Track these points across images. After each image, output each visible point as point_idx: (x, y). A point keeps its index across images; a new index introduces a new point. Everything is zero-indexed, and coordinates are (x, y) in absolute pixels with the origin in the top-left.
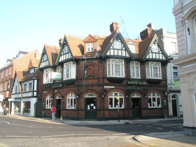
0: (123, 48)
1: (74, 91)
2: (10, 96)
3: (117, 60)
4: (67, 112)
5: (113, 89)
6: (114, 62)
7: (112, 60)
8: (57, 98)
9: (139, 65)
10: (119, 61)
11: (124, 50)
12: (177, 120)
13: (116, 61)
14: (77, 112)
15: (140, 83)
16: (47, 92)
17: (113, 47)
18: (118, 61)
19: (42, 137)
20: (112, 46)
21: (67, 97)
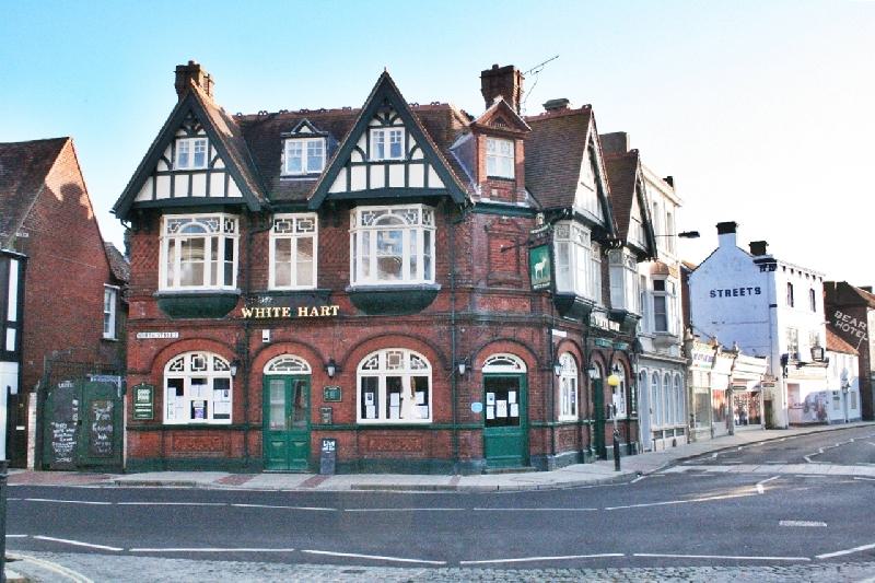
0: (414, 149)
4: (363, 439)
9: (433, 222)
12: (746, 484)
13: (190, 220)
14: (237, 438)
15: (303, 312)
16: (175, 335)
17: (170, 166)
18: (198, 220)
19: (825, 560)
20: (167, 161)
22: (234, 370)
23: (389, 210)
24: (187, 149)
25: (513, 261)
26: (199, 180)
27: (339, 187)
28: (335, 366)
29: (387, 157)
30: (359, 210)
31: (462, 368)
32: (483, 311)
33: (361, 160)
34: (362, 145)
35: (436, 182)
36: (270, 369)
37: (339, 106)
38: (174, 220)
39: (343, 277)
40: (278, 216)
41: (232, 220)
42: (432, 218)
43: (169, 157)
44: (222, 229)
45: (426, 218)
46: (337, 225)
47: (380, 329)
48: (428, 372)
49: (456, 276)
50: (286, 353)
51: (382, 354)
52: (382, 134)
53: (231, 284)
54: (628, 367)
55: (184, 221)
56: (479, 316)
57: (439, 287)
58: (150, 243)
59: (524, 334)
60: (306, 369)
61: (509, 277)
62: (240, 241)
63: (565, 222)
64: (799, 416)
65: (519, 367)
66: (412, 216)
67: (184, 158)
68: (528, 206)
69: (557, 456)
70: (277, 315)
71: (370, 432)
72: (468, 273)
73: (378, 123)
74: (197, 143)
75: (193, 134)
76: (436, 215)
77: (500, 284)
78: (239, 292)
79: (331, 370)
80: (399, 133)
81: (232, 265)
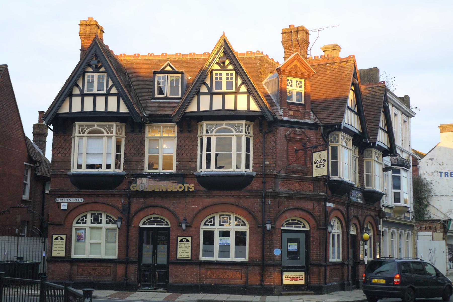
2: (438, 226)
3: (224, 122)
5: (81, 204)
6: (215, 130)
7: (80, 126)
8: (141, 225)
9: (124, 134)
11: (243, 93)
13: (94, 126)
16: (81, 200)
18: (98, 126)
20: (207, 86)
21: (75, 225)
22: (119, 224)
23: (96, 125)
24: (221, 78)
25: (303, 158)
26: (101, 101)
27: (193, 108)
29: (95, 91)
32: (282, 189)
33: (207, 91)
35: (124, 109)
36: (143, 224)
38: (82, 126)
39: (193, 165)
41: (249, 126)
43: (81, 86)
44: (244, 132)
45: (248, 130)
46: (189, 132)
47: (215, 200)
48: (246, 228)
49: (265, 166)
50: (154, 213)
52: (93, 76)
53: (119, 168)
54: (375, 226)
56: (280, 193)
57: (255, 174)
58: (65, 140)
59: (309, 205)
61: (299, 168)
63: (337, 133)
67: (91, 85)
69: (328, 285)
73: (91, 70)
74: (227, 74)
75: (97, 70)
78: (125, 173)
79: (184, 226)
80: (103, 76)
81: (249, 155)
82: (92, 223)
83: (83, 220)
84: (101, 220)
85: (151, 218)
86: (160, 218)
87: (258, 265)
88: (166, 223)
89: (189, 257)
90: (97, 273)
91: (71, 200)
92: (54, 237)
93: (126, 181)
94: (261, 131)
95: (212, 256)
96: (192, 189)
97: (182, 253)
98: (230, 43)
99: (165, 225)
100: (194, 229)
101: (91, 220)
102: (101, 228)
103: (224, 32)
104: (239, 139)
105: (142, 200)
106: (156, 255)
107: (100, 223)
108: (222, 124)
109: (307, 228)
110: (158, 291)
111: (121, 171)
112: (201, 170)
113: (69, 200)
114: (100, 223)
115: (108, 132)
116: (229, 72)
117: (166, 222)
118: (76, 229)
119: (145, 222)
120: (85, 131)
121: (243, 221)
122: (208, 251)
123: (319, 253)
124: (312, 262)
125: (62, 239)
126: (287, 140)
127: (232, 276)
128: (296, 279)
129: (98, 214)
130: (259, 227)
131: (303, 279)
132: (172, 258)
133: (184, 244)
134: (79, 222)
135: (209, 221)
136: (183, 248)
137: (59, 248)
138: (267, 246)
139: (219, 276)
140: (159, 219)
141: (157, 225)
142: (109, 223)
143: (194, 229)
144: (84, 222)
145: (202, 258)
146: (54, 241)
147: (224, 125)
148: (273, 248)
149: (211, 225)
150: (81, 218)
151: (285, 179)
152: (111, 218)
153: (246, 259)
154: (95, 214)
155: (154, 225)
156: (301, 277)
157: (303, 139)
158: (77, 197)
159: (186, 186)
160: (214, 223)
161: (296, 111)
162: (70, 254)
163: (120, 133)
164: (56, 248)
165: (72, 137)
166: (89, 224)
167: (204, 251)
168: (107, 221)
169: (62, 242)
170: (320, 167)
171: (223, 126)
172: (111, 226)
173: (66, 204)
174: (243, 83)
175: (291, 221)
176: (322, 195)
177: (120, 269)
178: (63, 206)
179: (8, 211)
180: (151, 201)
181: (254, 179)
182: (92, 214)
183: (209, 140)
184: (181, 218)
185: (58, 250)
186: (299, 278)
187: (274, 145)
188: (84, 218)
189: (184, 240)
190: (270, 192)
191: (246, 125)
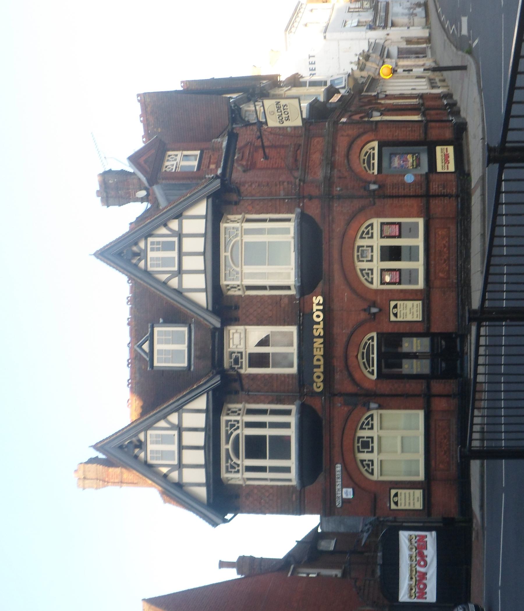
0: (169, 422)
1: (348, 223)
3: (223, 254)
4: (437, 283)
5: (345, 468)
8: (375, 377)
10: (228, 436)
11: (180, 419)
13: (227, 450)
16: (338, 468)
18: (227, 442)
20: (169, 279)
28: (370, 307)
30: (224, 475)
31: (373, 187)
32: (320, 174)
34: (164, 470)
36: (372, 373)
37: (128, 328)
38: (227, 468)
39: (286, 301)
40: (226, 365)
41: (229, 409)
42: (230, 217)
44: (238, 418)
45: (235, 412)
47: (336, 267)
50: (357, 357)
51: (360, 265)
55: (228, 457)
57: (299, 210)
59: (342, 143)
60: (372, 338)
62: (249, 403)
64: (420, 18)
65: (372, 338)
66: (232, 426)
67: (166, 262)
68: (227, 138)
70: (321, 307)
71: (432, 278)
72: (285, 184)
74: (152, 250)
76: (229, 214)
77: (296, 160)
78: (298, 402)
79: (374, 310)
82: (372, 451)
83: (368, 274)
84: (367, 437)
85: (364, 363)
86: (364, 348)
87: (428, 203)
88: (370, 341)
89: (420, 303)
90: (445, 441)
91: (338, 483)
92: (393, 507)
93: (309, 401)
94: (237, 392)
95: (417, 270)
96: (320, 299)
97: (413, 315)
98: (105, 245)
99: (373, 341)
100: (379, 297)
101: (367, 452)
102: (379, 438)
103: (90, 447)
104: (248, 232)
105: (337, 376)
106: (417, 354)
107: (372, 438)
108: (225, 257)
109: (375, 144)
110: (469, 350)
111: (293, 408)
112: (293, 288)
113: (338, 487)
114: (372, 438)
115: (236, 427)
116: (149, 246)
117: (369, 340)
118: (381, 475)
119: (369, 371)
120: (235, 463)
121: (367, 419)
122: (410, 277)
123: (410, 129)
124: (423, 136)
125: (396, 495)
126: (250, 169)
127: (444, 242)
128: (447, 157)
129: (358, 442)
130: (374, 204)
131: (447, 149)
132: (420, 329)
133: (400, 311)
134: (370, 471)
135: (366, 277)
136: (406, 313)
137: (409, 499)
138: (402, 192)
139: (445, 261)
140: (365, 351)
141: (373, 353)
142: (372, 425)
143: (379, 297)
144: (370, 272)
145: (421, 285)
146: (399, 507)
147: (226, 254)
148: (404, 184)
149: (372, 274)
150: (365, 468)
151: (305, 171)
152: (363, 423)
153: (421, 222)
154: (358, 447)
155: (373, 358)
156: (444, 167)
157: (250, 150)
158: (335, 475)
159: (315, 308)
160: (369, 269)
161: (210, 161)
162: (419, 482)
163: (237, 274)
164: (409, 503)
165: (244, 485)
166: (374, 456)
167: (410, 282)
168: (369, 429)
169: (401, 495)
170: (288, 114)
171: (228, 256)
172: (376, 422)
173: (344, 490)
174: (165, 225)
175: (365, 360)
176: (329, 125)
177: (439, 404)
178: (347, 495)
179: (356, 582)
180: (338, 363)
181: (306, 212)
182: (359, 452)
183: (249, 469)
184: (363, 316)
185: (414, 499)
186: (445, 153)
187: (257, 184)
188: (364, 463)
189: (395, 311)
190: (324, 187)
191: (228, 414)
